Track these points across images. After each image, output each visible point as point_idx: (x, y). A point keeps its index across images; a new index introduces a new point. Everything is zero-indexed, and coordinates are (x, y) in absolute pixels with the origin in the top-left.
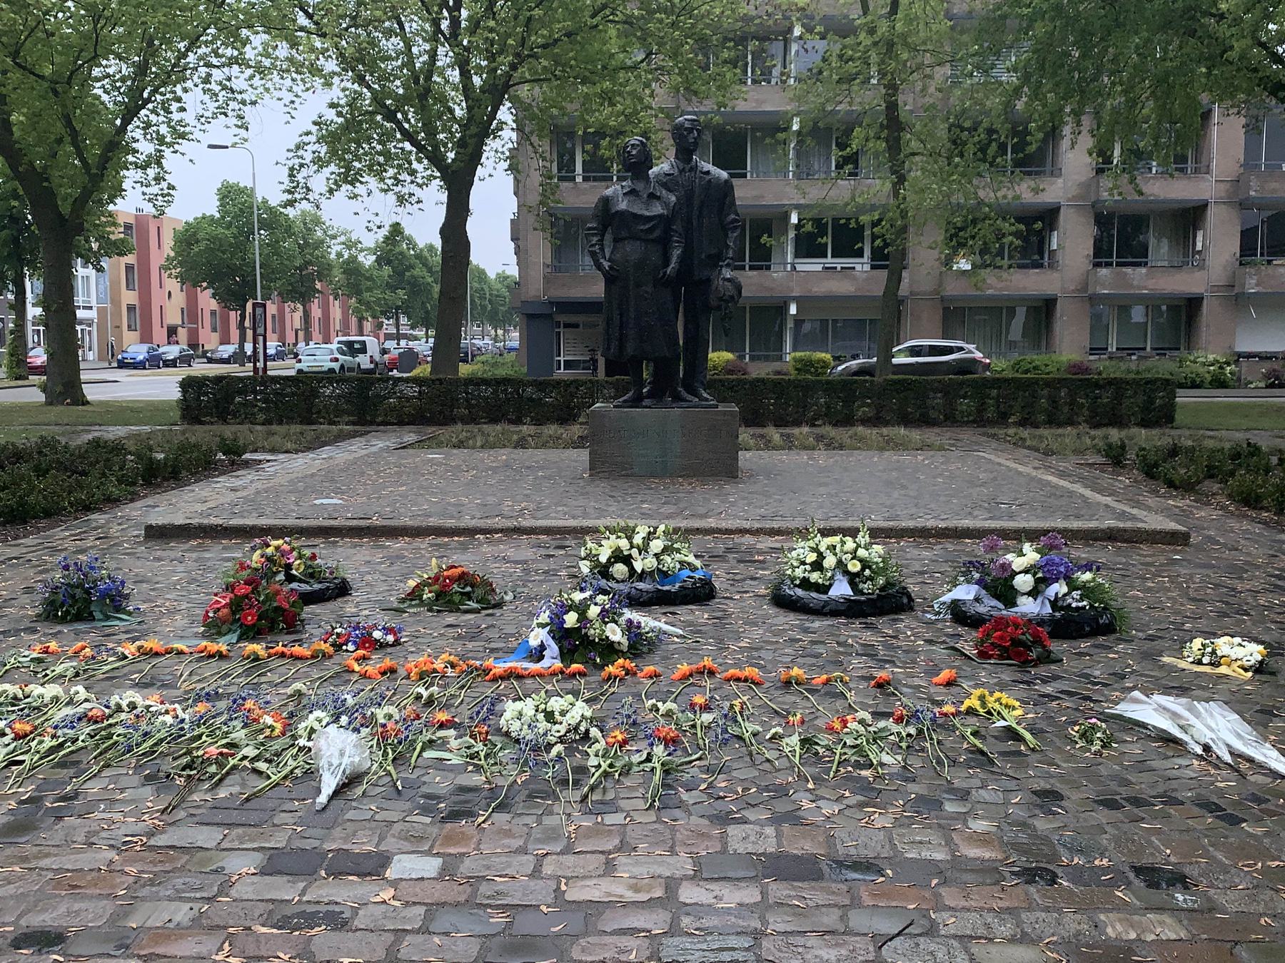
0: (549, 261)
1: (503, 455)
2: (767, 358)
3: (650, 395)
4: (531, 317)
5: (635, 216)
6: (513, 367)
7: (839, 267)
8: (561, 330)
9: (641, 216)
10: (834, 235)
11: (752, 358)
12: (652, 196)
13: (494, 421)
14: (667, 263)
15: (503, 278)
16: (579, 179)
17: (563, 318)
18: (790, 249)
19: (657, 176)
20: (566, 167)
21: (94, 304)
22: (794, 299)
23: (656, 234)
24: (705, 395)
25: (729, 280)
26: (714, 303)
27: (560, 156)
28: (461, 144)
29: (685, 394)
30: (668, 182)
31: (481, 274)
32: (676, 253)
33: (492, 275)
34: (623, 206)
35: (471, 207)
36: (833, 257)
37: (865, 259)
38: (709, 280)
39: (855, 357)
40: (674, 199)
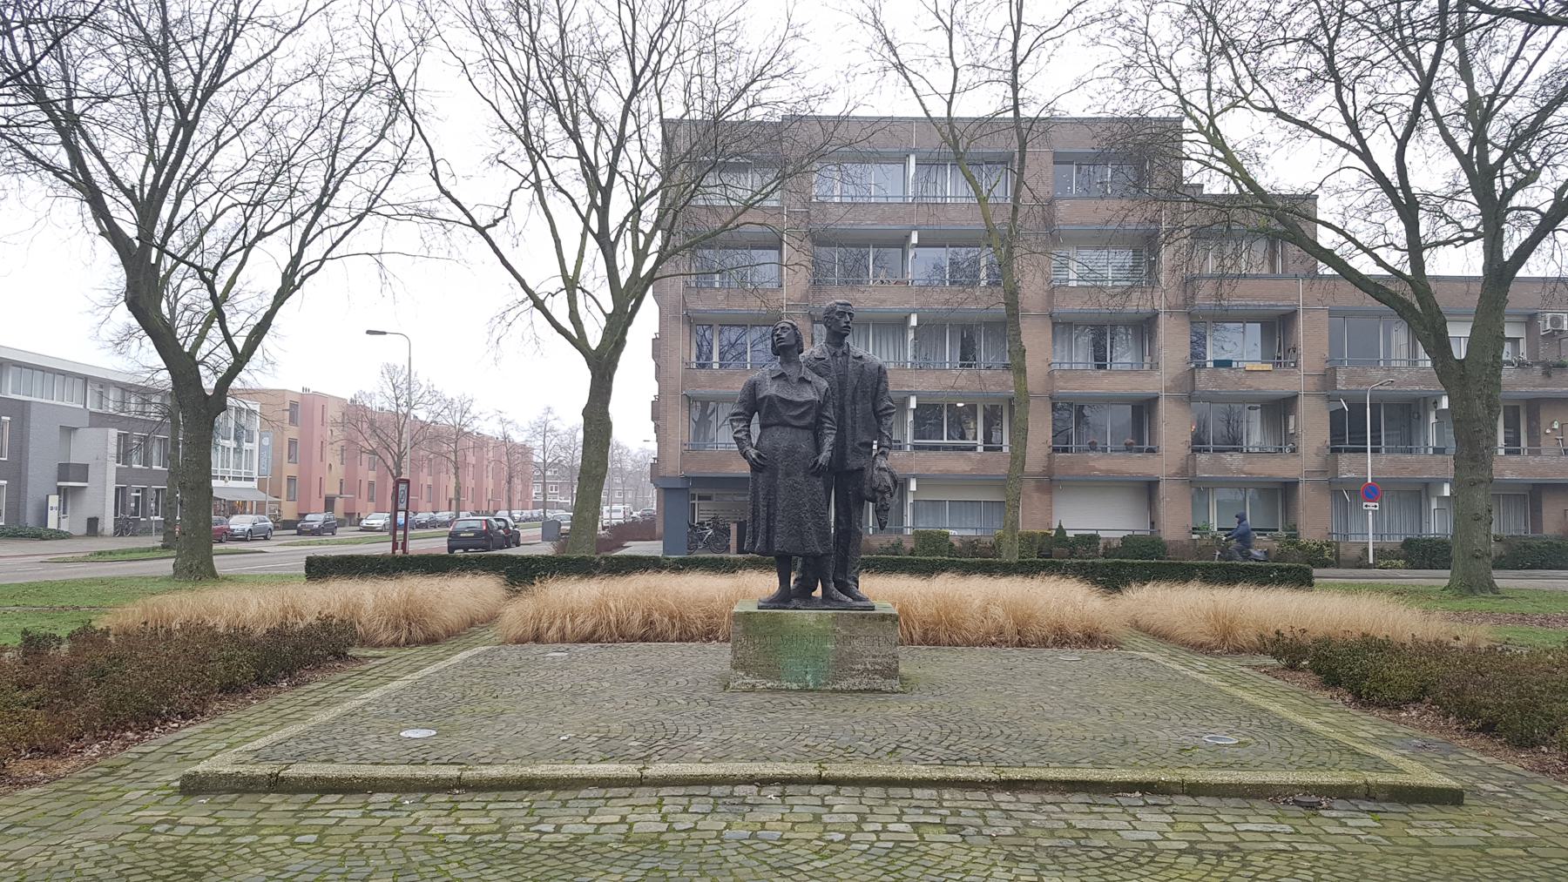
5: (782, 400)
14: (818, 451)
17: (697, 492)
21: (255, 475)
23: (809, 420)
26: (867, 493)
30: (819, 367)
32: (829, 440)
38: (861, 470)
40: (825, 384)
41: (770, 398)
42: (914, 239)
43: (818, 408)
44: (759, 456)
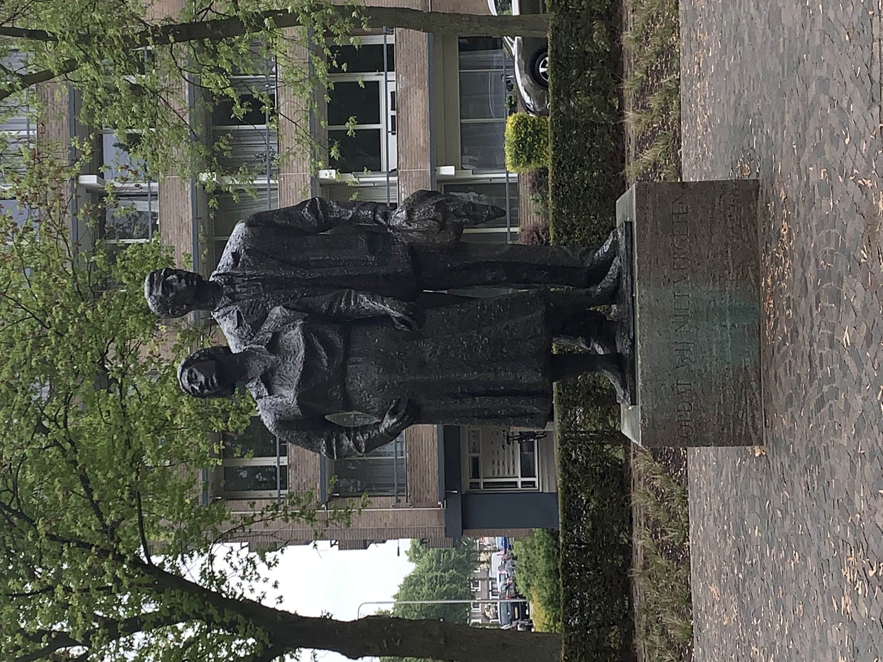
0: (392, 500)
1: (706, 590)
2: (515, 203)
3: (609, 341)
4: (465, 527)
6: (532, 543)
7: (391, 113)
8: (482, 481)
9: (305, 364)
10: (350, 120)
11: (514, 224)
12: (274, 345)
13: (627, 588)
14: (385, 318)
15: (415, 554)
16: (284, 461)
17: (467, 479)
18: (368, 178)
19: (242, 340)
20: (274, 479)
22: (434, 170)
23: (338, 341)
24: (606, 248)
25: (410, 214)
26: (449, 238)
27: (260, 486)
28: (233, 628)
29: (608, 280)
30: (251, 321)
31: (411, 584)
32: (367, 303)
33: (409, 568)
34: (289, 395)
35: (317, 614)
36: (378, 122)
37: (381, 79)
38: (412, 249)
39: (511, 85)
40: (277, 310)
41: (301, 398)
42: (90, 180)
43: (315, 324)
44: (393, 413)
